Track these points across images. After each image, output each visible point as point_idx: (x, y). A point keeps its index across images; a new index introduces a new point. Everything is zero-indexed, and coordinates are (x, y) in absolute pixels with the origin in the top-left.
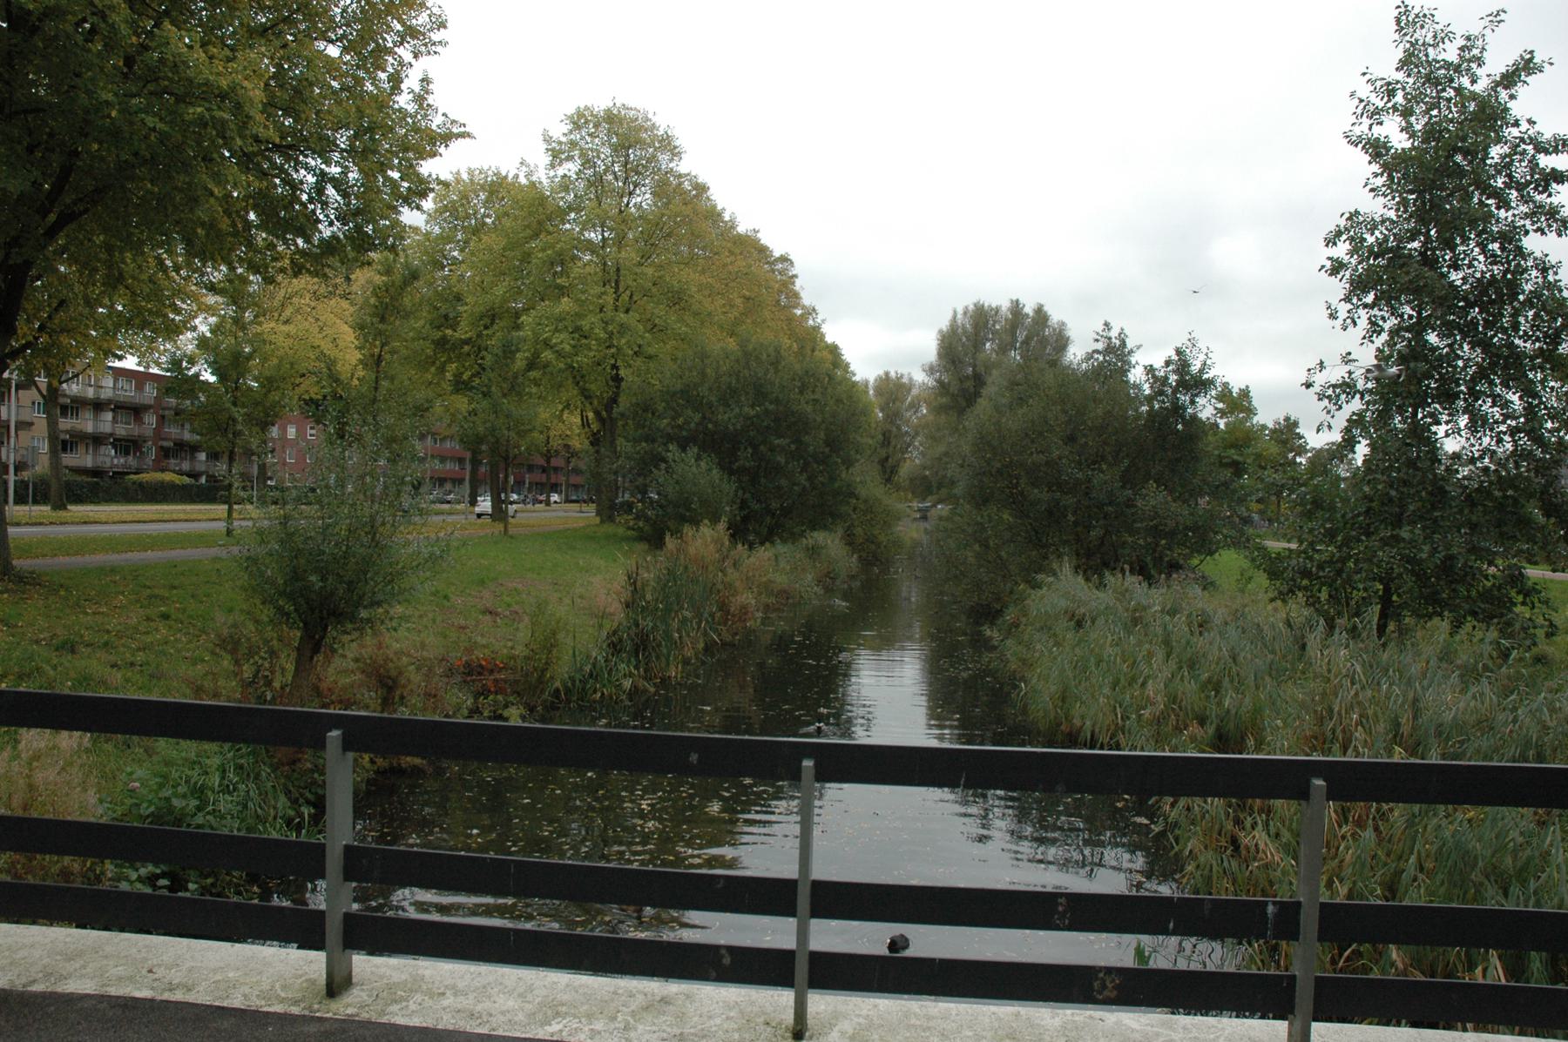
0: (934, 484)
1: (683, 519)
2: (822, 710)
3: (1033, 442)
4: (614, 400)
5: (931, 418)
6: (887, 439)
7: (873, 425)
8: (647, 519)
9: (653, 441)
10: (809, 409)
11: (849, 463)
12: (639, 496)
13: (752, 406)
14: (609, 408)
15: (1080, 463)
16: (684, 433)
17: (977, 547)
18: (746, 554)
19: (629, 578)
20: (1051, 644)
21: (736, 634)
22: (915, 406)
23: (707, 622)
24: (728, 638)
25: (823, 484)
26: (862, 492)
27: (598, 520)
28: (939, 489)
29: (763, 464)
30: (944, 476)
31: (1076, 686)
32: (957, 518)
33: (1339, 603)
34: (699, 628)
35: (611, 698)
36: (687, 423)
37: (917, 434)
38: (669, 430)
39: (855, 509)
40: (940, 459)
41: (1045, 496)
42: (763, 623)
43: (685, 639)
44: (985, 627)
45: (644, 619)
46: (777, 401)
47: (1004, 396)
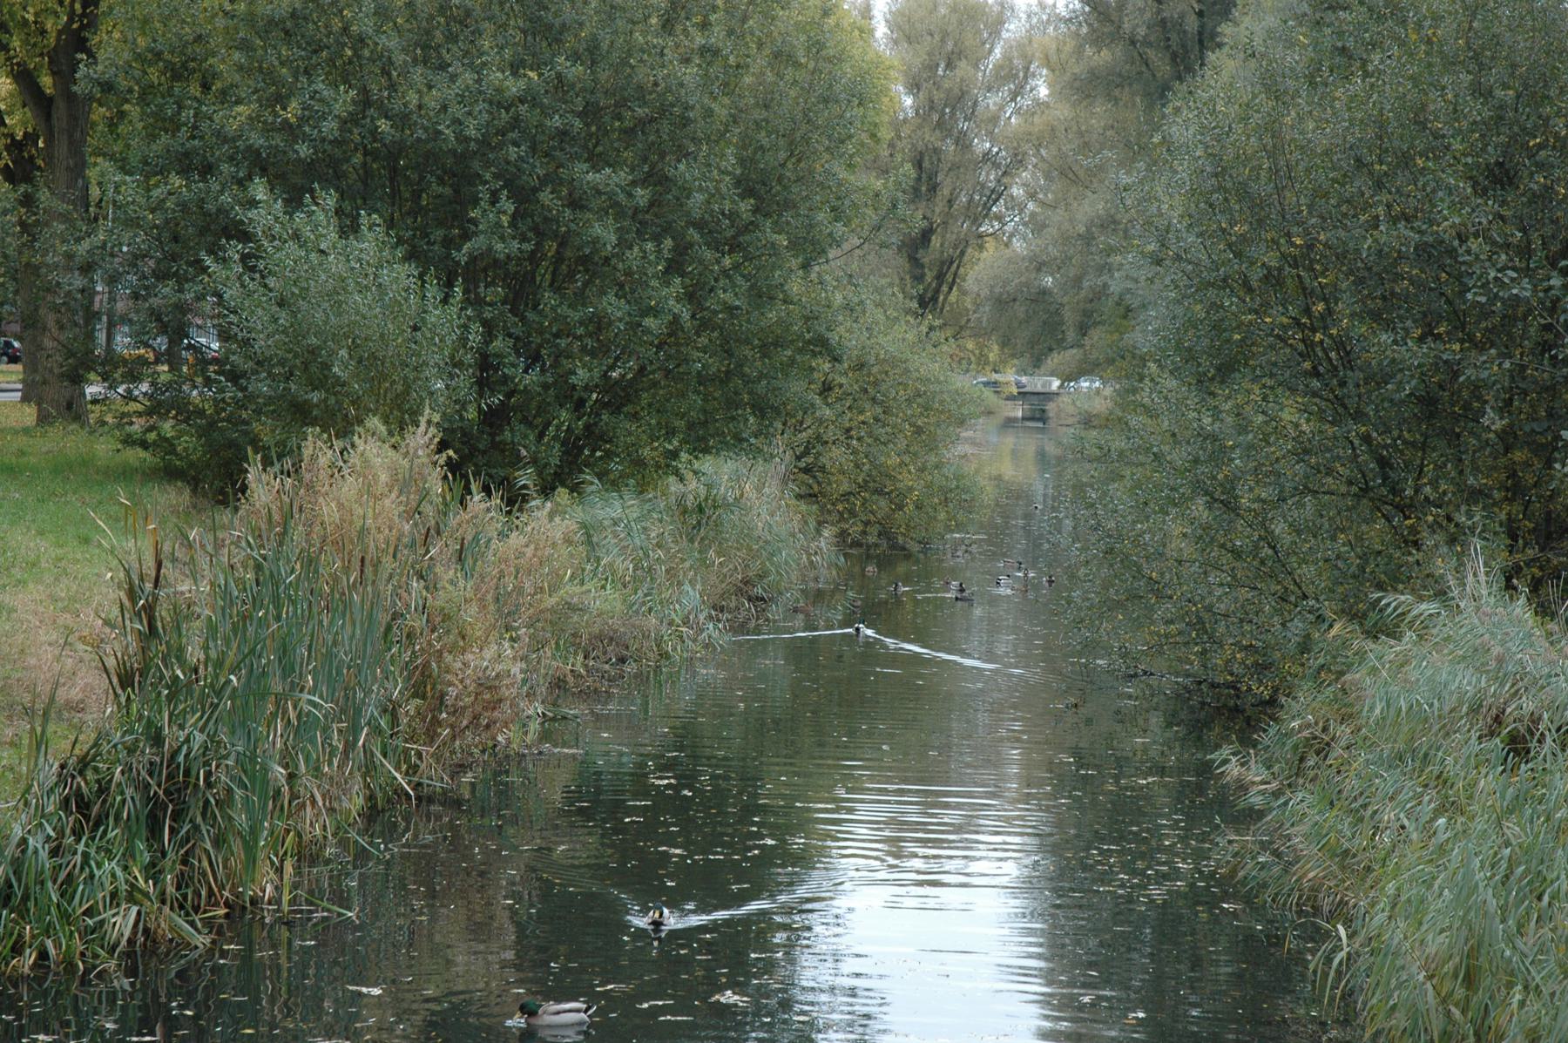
0: (1069, 316)
1: (301, 414)
2: (729, 997)
3: (1379, 185)
4: (77, 41)
5: (1063, 112)
6: (925, 183)
7: (886, 134)
8: (186, 413)
9: (207, 170)
10: (690, 74)
11: (810, 249)
12: (161, 343)
13: (515, 68)
14: (64, 73)
15: (1525, 251)
16: (304, 150)
17: (1199, 508)
18: (496, 520)
19: (132, 595)
20: (1428, 808)
21: (462, 768)
22: (1014, 76)
23: (376, 730)
24: (436, 778)
25: (730, 310)
26: (848, 336)
27: (29, 414)
28: (1083, 330)
29: (551, 247)
30: (1100, 293)
31: (1510, 940)
32: (1135, 421)
33: (87, 818)
34: (350, 746)
35: (71, 966)
36: (310, 117)
37: (1019, 161)
38: (257, 140)
39: (826, 388)
40: (1088, 239)
41: (1415, 354)
42: (545, 736)
43: (307, 782)
44: (1225, 751)
45: (178, 720)
46: (591, 54)
47: (1291, 44)
